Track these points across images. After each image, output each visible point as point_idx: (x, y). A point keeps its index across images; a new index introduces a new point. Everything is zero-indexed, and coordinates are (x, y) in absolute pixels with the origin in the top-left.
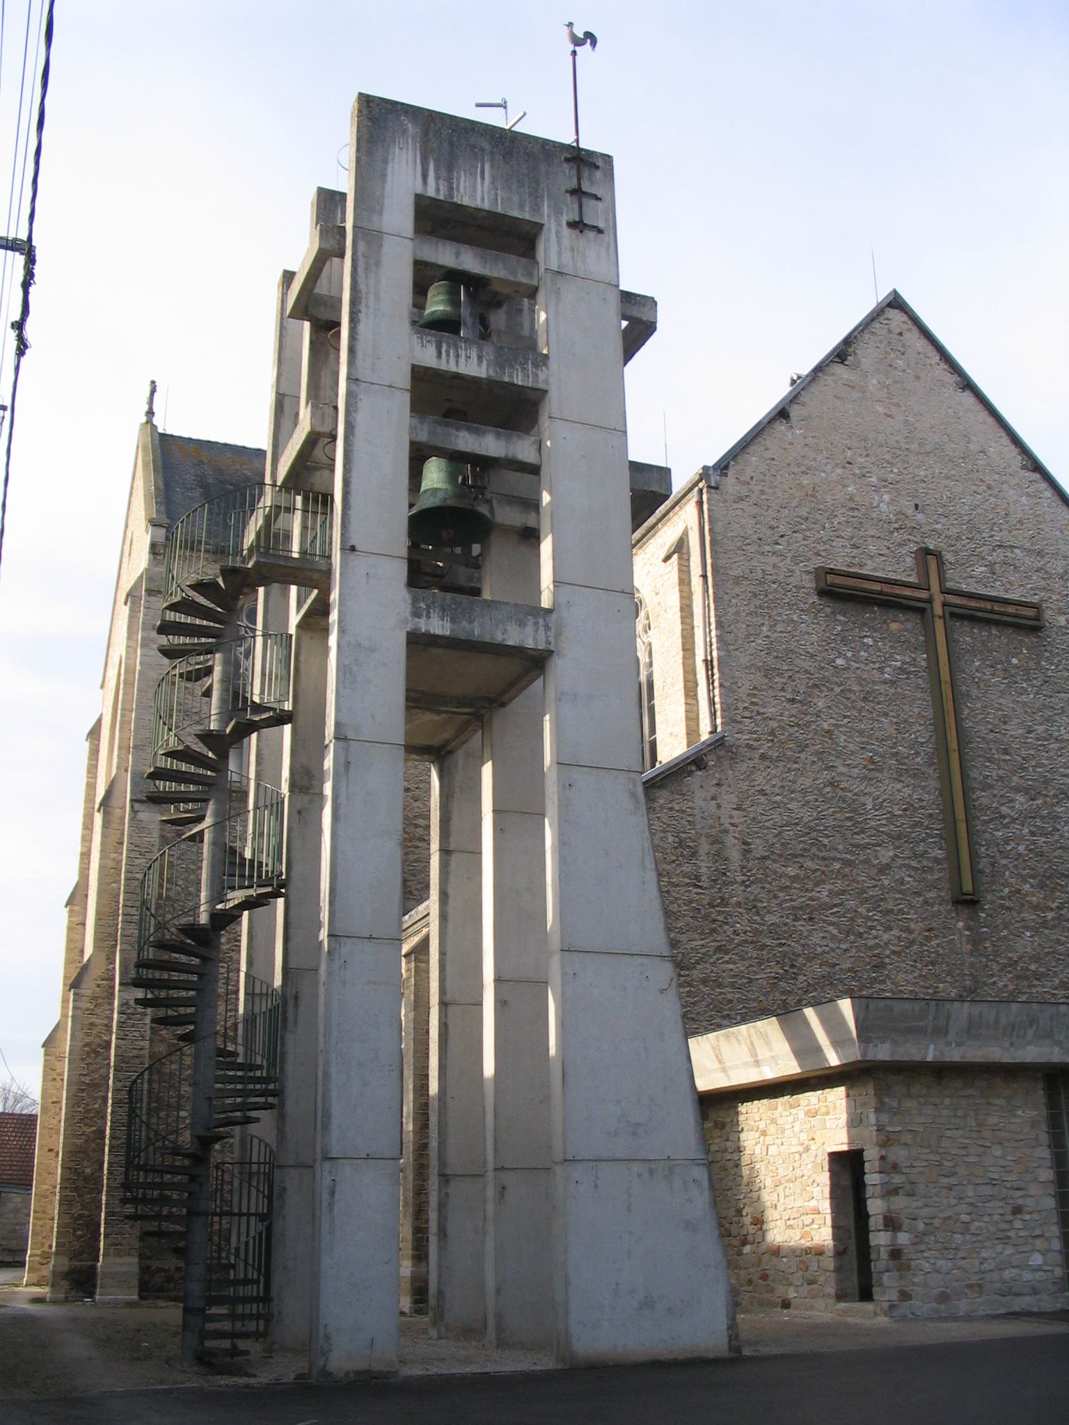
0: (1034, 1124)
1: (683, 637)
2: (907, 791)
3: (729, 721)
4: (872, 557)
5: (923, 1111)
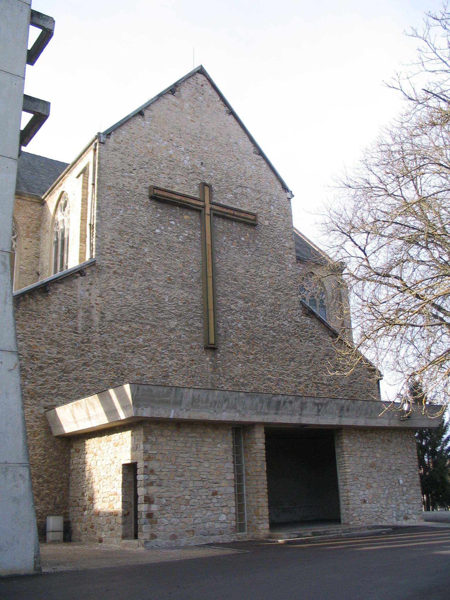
0: (226, 451)
1: (82, 213)
2: (186, 294)
3: (100, 253)
4: (178, 184)
5: (168, 443)
